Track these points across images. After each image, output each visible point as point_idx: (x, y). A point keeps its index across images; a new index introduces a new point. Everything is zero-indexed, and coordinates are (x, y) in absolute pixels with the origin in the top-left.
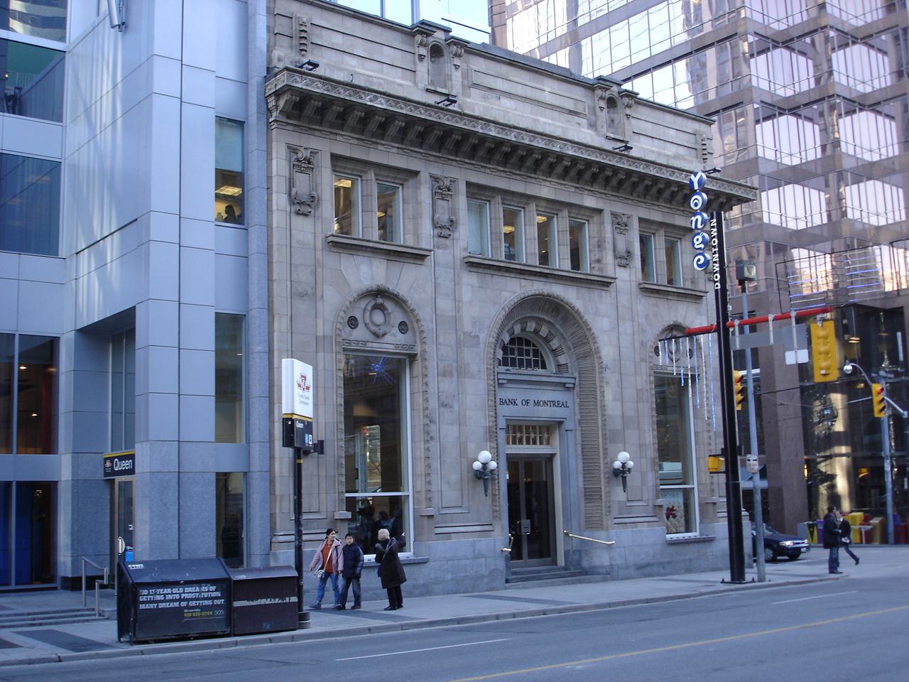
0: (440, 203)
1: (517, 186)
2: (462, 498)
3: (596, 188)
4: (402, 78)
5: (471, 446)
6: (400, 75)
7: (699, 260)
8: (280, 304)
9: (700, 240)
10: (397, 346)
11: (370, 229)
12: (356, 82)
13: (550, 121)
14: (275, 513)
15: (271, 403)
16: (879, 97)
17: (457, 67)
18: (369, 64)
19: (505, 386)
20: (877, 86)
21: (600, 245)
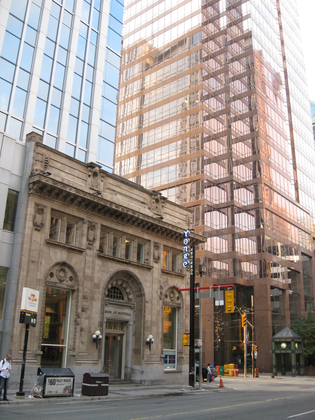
0: (90, 231)
1: (120, 228)
5: (93, 329)
6: (81, 181)
7: (185, 263)
8: (24, 266)
9: (186, 256)
10: (68, 286)
11: (63, 239)
12: (64, 182)
13: (134, 205)
14: (12, 350)
15: (16, 305)
16: (249, 208)
17: (102, 181)
18: (69, 176)
19: (108, 305)
20: (249, 203)
21: (148, 254)
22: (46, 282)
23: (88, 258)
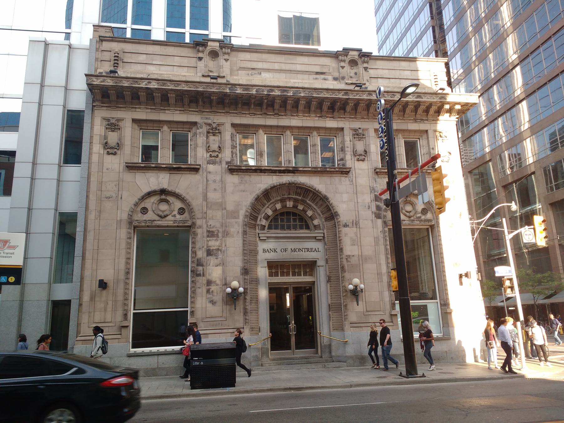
0: (212, 138)
1: (272, 121)
2: (223, 312)
4: (188, 72)
10: (175, 221)
13: (301, 81)
17: (226, 60)
19: (267, 241)
21: (343, 150)
22: (130, 223)
23: (211, 177)
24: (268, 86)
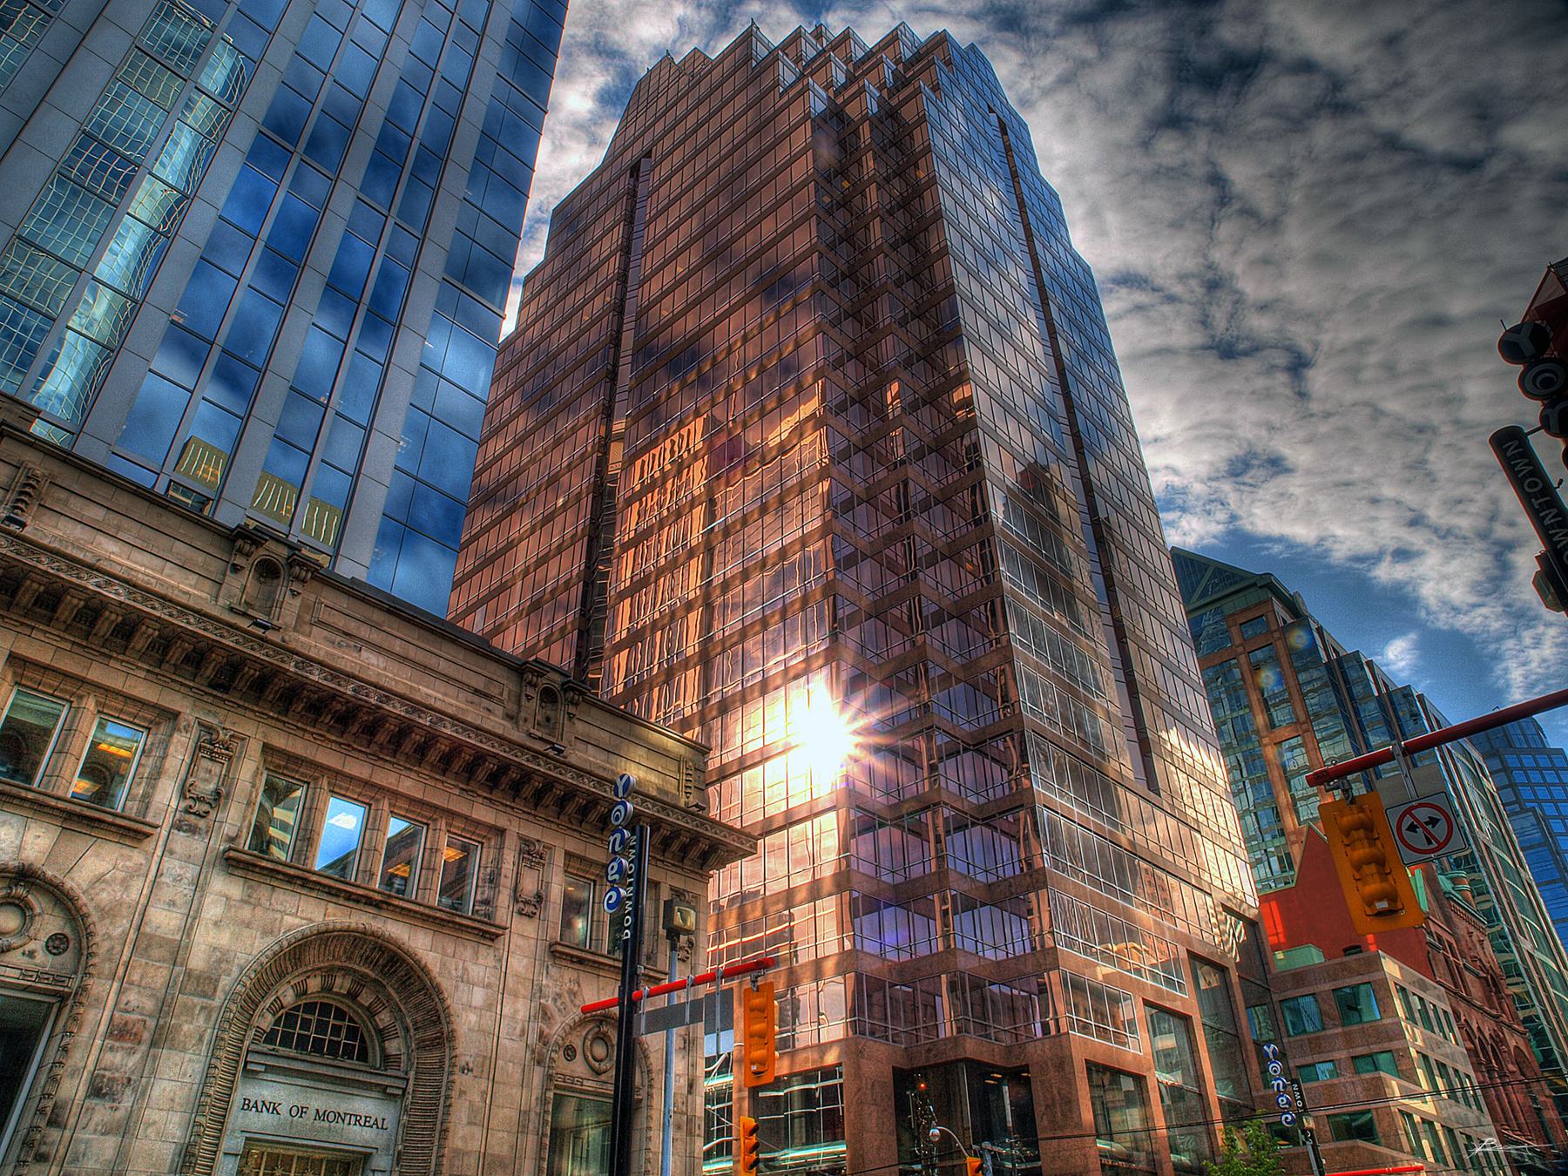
3: (497, 795)
7: (611, 897)
10: (25, 973)
13: (440, 696)
21: (493, 880)
23: (172, 866)
24: (382, 688)
